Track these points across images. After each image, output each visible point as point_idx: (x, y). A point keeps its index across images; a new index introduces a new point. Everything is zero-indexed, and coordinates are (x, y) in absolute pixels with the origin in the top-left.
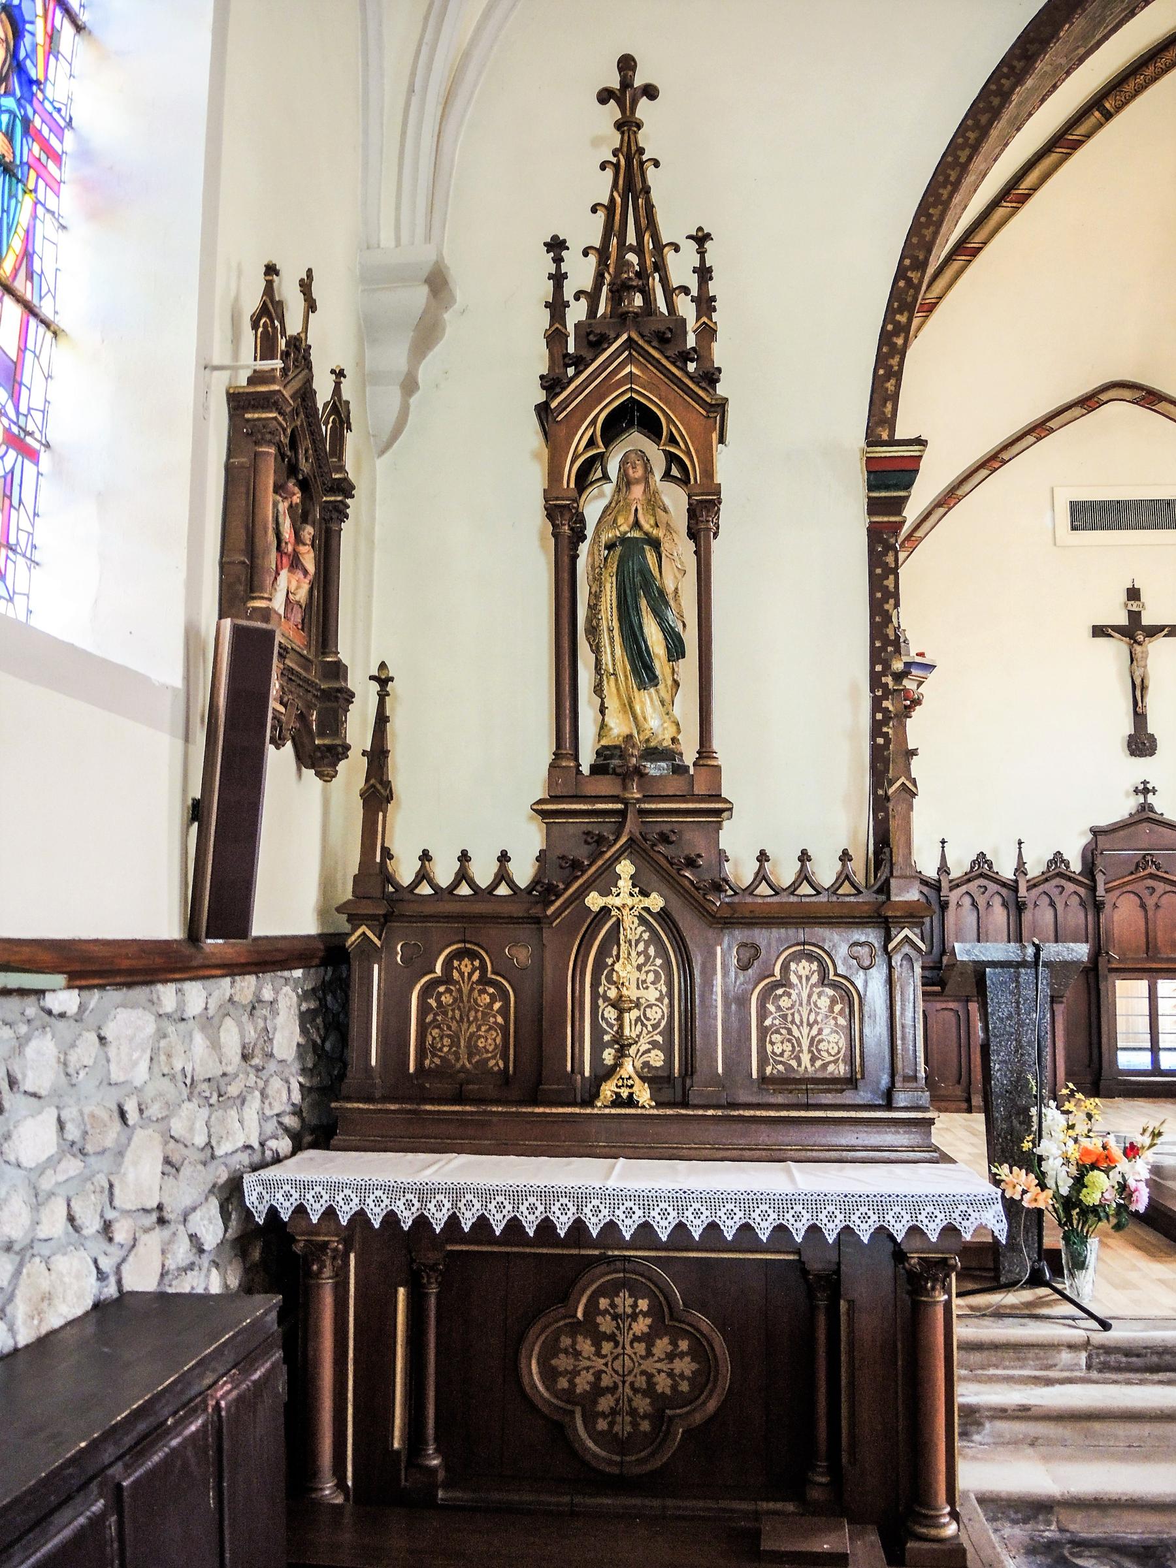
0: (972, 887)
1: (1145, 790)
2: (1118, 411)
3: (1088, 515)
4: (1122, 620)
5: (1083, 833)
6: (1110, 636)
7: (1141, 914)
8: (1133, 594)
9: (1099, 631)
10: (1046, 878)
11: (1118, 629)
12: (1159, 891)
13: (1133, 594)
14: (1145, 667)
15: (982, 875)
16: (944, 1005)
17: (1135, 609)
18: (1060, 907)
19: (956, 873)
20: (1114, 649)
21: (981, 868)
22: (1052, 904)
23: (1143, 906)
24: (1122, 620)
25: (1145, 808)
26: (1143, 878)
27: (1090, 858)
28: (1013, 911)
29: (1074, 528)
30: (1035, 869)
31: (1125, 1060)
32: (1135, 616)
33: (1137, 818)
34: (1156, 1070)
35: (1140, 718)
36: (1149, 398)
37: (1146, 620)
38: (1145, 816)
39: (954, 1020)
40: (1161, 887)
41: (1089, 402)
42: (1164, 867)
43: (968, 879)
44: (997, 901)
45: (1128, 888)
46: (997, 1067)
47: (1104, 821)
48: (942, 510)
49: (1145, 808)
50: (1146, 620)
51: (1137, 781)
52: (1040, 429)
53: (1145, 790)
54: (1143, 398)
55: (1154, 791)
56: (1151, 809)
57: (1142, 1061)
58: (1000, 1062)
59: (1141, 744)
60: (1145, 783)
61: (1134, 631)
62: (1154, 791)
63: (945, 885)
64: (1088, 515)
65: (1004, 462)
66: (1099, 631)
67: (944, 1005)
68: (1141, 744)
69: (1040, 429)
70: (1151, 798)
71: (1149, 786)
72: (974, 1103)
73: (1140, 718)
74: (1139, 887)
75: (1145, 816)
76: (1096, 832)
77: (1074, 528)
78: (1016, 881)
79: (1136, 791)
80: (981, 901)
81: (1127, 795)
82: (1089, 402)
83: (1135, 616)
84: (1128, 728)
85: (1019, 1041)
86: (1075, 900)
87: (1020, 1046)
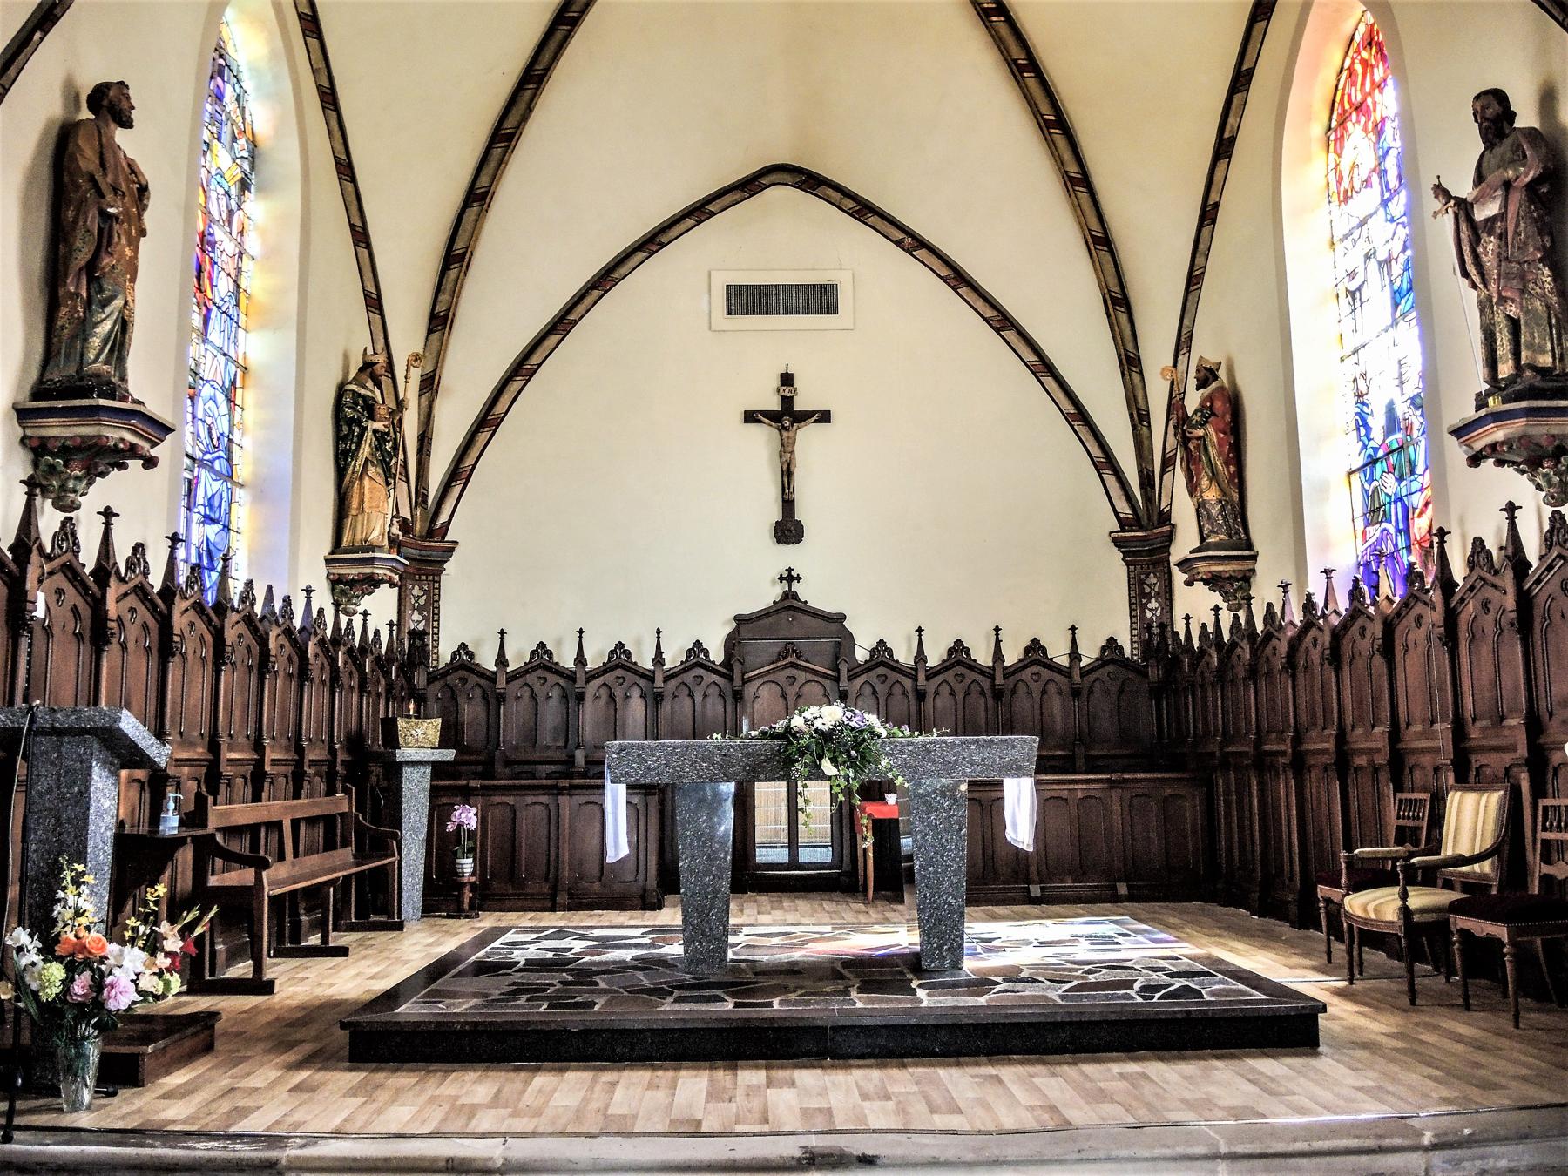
0: (608, 678)
1: (790, 577)
2: (780, 196)
3: (743, 300)
4: (774, 405)
5: (726, 623)
6: (760, 421)
7: (781, 702)
8: (787, 379)
9: (750, 417)
10: (685, 668)
11: (766, 414)
12: (801, 680)
13: (787, 379)
14: (792, 452)
15: (959, 663)
16: (535, 799)
17: (787, 394)
18: (698, 698)
19: (593, 663)
20: (763, 437)
21: (619, 658)
22: (691, 695)
23: (784, 696)
24: (774, 405)
25: (790, 595)
26: (784, 668)
27: (732, 643)
28: (729, 700)
29: (729, 312)
30: (594, 660)
31: (762, 856)
32: (787, 402)
33: (779, 606)
34: (793, 863)
35: (788, 505)
36: (810, 181)
37: (799, 406)
38: (789, 604)
39: (545, 814)
40: (802, 676)
41: (750, 186)
42: (806, 655)
43: (605, 670)
44: (636, 693)
45: (770, 678)
46: (34, 847)
47: (748, 609)
48: (596, 293)
49: (790, 595)
50: (799, 406)
51: (781, 569)
52: (699, 212)
53: (790, 577)
54: (804, 182)
55: (799, 578)
56: (795, 596)
57: (781, 856)
58: (38, 842)
59: (788, 531)
60: (790, 570)
61: (786, 417)
62: (799, 578)
63: (580, 677)
64: (743, 300)
65: (663, 245)
66: (750, 417)
67: (535, 799)
68: (788, 531)
69: (699, 212)
70: (795, 586)
71: (794, 574)
72: (559, 900)
73: (788, 505)
74: (782, 676)
75: (789, 604)
76: (739, 619)
77: (729, 312)
78: (916, 670)
79: (781, 579)
80: (619, 693)
81: (773, 583)
82: (750, 186)
83: (787, 402)
84: (776, 514)
85: (58, 819)
86: (714, 690)
87: (58, 823)
